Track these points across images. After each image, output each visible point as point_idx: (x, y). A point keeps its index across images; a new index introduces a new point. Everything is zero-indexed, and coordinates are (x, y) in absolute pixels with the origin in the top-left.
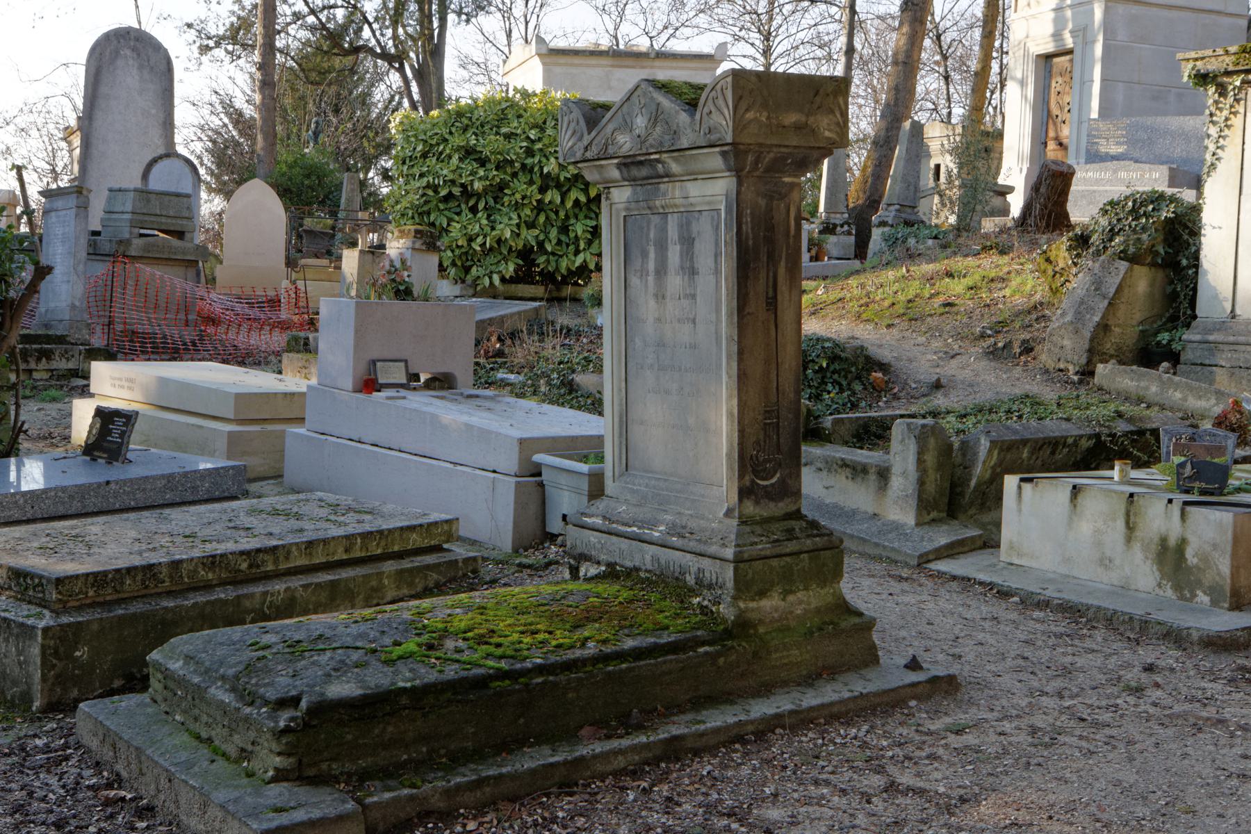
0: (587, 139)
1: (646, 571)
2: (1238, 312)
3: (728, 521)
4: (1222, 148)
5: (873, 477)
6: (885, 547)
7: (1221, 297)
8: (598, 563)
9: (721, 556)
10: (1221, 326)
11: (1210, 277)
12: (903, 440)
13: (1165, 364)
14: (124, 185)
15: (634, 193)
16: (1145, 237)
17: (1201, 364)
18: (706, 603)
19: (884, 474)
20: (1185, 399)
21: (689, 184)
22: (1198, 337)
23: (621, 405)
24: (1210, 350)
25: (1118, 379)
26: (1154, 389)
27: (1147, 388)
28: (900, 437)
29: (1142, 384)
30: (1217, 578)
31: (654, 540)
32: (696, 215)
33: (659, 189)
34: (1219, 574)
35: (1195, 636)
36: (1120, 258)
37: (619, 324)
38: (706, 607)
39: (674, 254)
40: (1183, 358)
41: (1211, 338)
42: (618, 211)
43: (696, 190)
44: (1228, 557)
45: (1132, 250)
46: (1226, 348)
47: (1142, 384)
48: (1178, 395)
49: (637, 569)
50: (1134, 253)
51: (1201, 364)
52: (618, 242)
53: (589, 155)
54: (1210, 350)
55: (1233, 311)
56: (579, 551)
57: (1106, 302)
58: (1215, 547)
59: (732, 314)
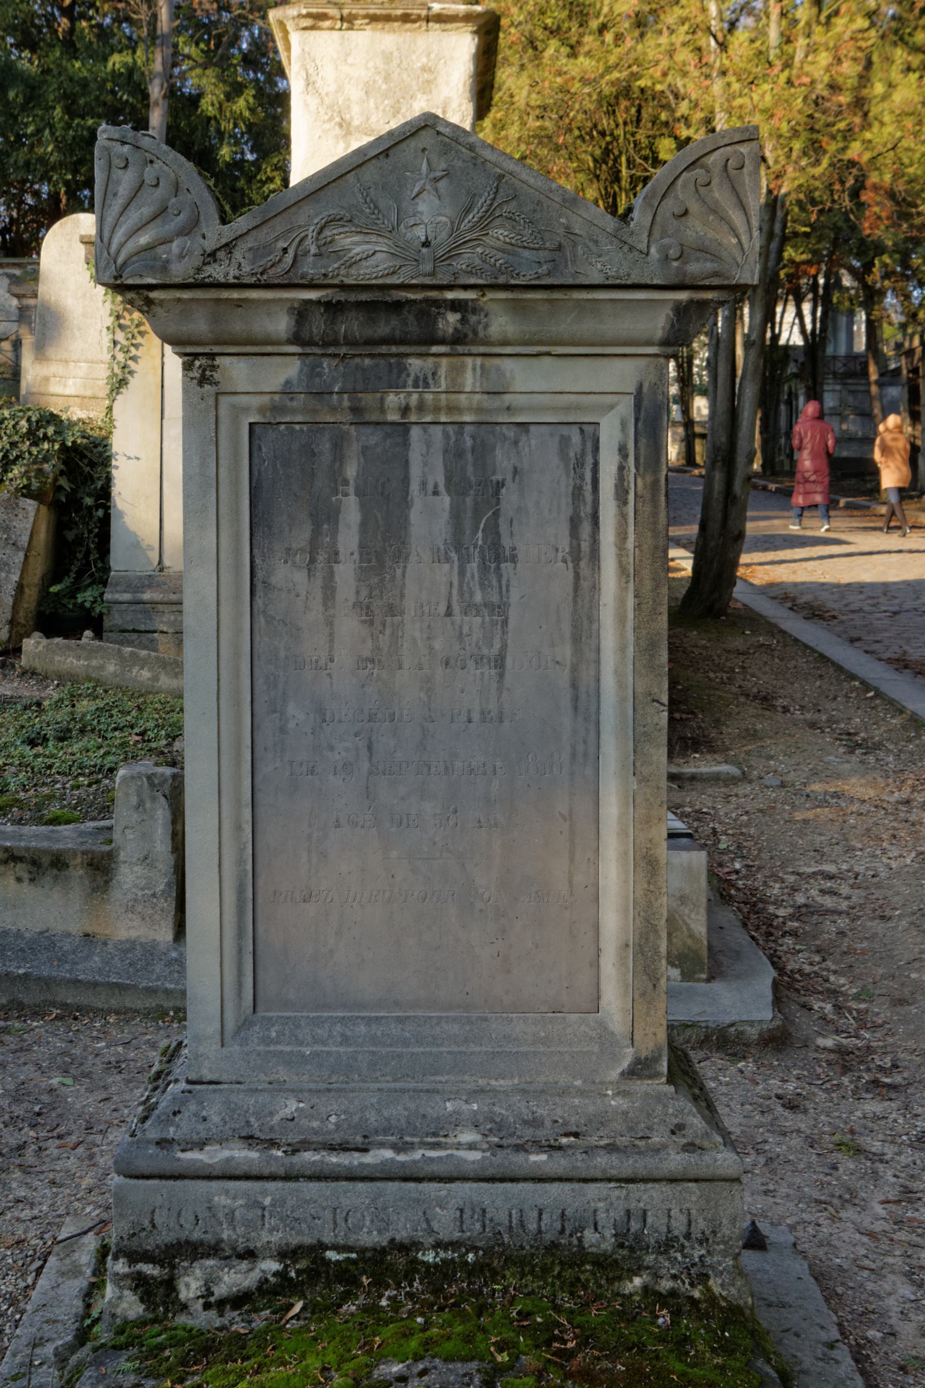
0: (214, 233)
1: (438, 1245)
2: (167, 562)
3: (641, 1086)
4: (134, 359)
5: (77, 872)
6: (167, 992)
7: (144, 544)
8: (250, 1255)
9: (703, 1172)
10: (149, 582)
11: (127, 520)
12: (140, 804)
13: (88, 633)
14: (328, 32)
15: (313, 372)
16: (47, 467)
17: (134, 631)
18: (666, 1285)
19: (101, 867)
20: (156, 679)
21: (508, 364)
22: (127, 597)
23: (240, 862)
24: (145, 612)
25: (57, 658)
26: (111, 668)
27: (102, 668)
28: (134, 800)
29: (94, 663)
30: (689, 942)
31: (469, 1170)
32: (511, 433)
33: (402, 369)
34: (692, 936)
35: (753, 1033)
36: (23, 495)
37: (236, 675)
38: (673, 1293)
39: (429, 518)
40: (107, 623)
41: (147, 596)
42: (238, 411)
43: (536, 384)
44: (703, 911)
45: (35, 485)
46: (167, 609)
47: (94, 663)
48: (146, 674)
49: (406, 1248)
50: (40, 489)
51: (134, 631)
52: (236, 482)
53: (217, 272)
54: (145, 612)
55: (160, 562)
56: (166, 1237)
57: (21, 555)
58: (683, 899)
59: (652, 645)
